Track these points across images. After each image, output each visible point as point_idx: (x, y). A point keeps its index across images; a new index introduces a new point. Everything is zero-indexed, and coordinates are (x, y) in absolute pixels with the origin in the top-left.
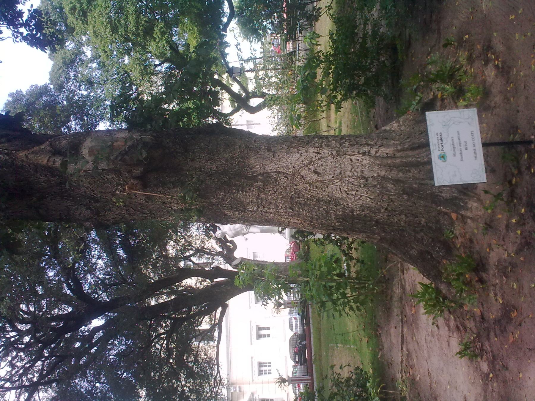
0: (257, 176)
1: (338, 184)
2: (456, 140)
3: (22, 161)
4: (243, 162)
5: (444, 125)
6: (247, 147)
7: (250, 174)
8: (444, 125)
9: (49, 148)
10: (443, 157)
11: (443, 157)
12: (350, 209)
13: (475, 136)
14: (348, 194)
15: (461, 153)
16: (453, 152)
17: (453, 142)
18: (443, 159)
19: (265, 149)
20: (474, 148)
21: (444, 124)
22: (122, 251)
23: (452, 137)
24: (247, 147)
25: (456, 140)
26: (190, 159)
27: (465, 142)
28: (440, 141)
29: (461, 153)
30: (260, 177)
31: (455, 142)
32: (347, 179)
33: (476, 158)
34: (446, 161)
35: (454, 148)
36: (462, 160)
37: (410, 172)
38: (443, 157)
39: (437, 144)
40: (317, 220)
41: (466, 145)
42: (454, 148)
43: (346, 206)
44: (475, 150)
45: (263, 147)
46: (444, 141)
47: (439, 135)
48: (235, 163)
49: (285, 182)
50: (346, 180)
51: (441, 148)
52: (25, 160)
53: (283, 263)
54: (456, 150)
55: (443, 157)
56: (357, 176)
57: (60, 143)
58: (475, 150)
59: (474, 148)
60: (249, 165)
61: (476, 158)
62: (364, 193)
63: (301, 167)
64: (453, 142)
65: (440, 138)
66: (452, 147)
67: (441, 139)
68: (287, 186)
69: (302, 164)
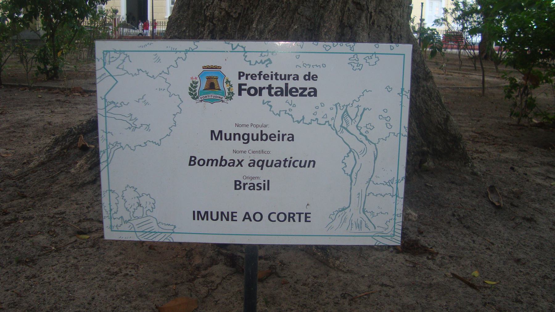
13: (287, 226)
15: (222, 162)
16: (227, 130)
17: (271, 137)
18: (203, 84)
20: (240, 216)
21: (352, 112)
28: (281, 84)
29: (222, 162)
33: (198, 215)
34: (195, 97)
35: (246, 138)
36: (193, 161)
38: (212, 86)
41: (252, 187)
42: (246, 138)
44: (231, 217)
46: (280, 102)
47: (309, 84)
51: (250, 83)
54: (238, 144)
55: (212, 86)
58: (231, 217)
59: (240, 216)
64: (271, 137)
65: (292, 84)
67: (286, 92)
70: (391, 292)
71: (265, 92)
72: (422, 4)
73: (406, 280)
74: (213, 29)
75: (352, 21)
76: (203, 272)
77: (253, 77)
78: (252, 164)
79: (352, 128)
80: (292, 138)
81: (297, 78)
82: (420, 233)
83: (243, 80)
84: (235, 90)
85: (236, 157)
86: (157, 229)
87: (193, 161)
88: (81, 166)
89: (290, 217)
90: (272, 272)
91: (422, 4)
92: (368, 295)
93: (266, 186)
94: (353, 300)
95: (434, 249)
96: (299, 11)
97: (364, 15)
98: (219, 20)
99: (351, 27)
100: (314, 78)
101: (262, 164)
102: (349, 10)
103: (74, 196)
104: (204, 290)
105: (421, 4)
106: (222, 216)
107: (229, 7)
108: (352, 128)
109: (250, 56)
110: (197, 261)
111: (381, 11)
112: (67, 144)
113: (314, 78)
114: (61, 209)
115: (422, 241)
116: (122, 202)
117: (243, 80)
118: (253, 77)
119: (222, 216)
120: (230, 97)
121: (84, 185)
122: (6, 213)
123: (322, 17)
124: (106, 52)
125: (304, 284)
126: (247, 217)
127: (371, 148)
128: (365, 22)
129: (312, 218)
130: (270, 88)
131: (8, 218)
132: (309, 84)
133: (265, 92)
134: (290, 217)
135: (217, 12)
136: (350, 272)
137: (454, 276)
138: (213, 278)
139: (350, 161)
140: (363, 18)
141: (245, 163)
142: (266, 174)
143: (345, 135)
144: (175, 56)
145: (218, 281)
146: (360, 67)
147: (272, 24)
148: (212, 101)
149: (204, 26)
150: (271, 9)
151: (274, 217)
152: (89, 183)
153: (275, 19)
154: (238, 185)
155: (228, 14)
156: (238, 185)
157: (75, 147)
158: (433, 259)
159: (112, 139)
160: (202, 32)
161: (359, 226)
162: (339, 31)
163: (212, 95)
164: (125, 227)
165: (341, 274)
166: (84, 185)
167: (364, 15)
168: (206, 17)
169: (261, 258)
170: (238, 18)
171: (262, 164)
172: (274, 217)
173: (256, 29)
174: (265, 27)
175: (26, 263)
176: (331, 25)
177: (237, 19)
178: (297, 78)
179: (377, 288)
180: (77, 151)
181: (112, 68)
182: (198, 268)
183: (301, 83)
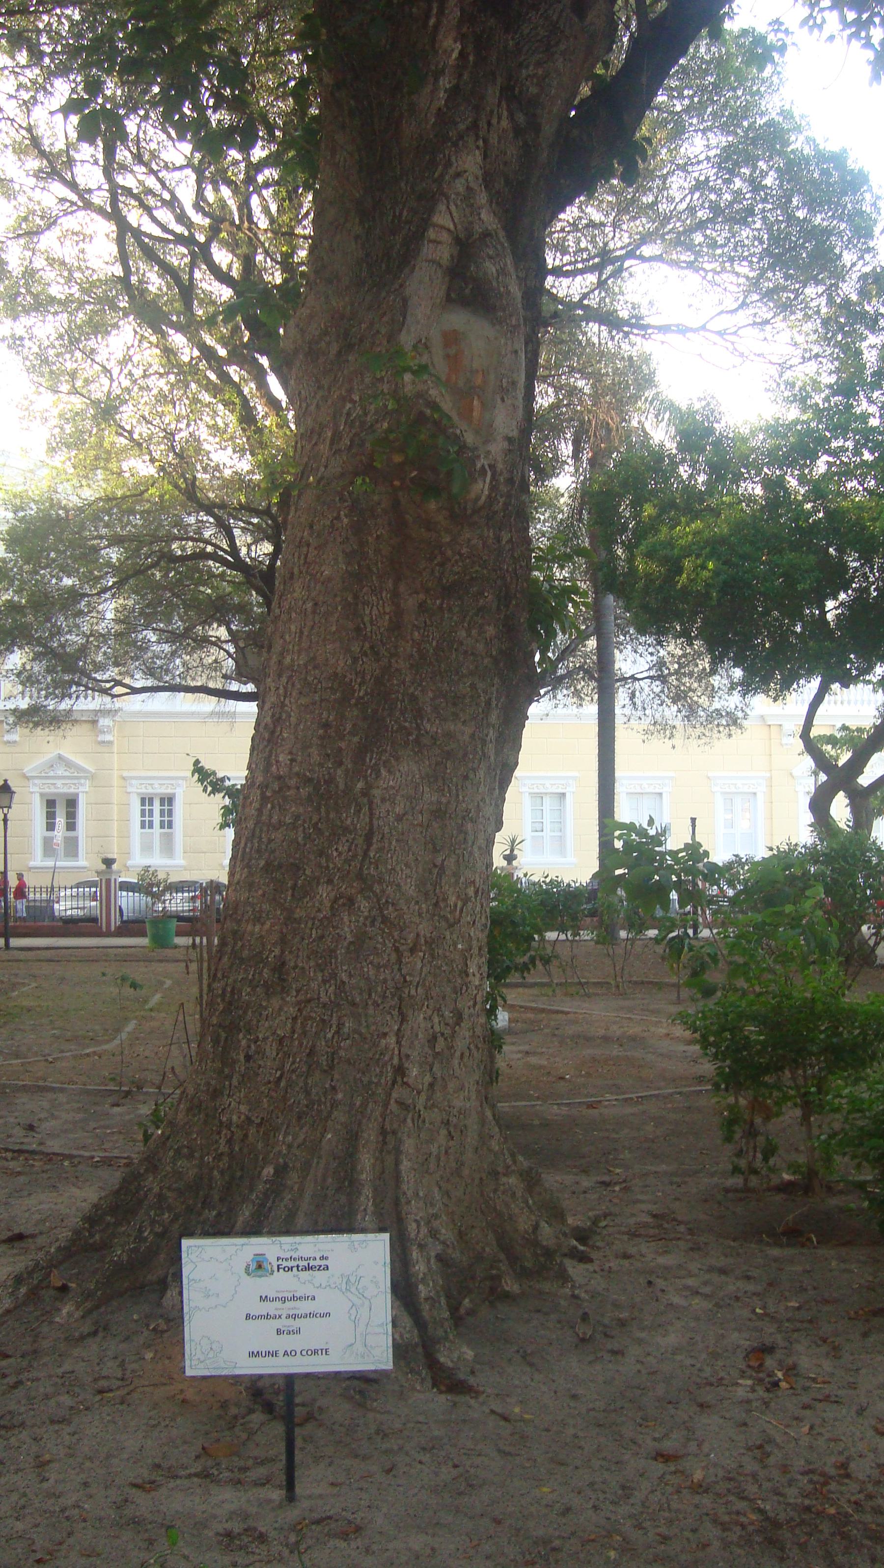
0: (365, 777)
1: (322, 994)
2: (304, 1307)
3: (448, 164)
4: (407, 743)
5: (348, 1280)
6: (449, 755)
7: (370, 759)
8: (348, 1280)
9: (478, 229)
10: (259, 1266)
11: (259, 1266)
12: (255, 1022)
13: (314, 1359)
14: (295, 1019)
15: (268, 1317)
16: (272, 1295)
17: (300, 1298)
18: (253, 1266)
19: (440, 803)
20: (281, 1353)
21: (353, 1279)
22: (864, 357)
23: (314, 1298)
24: (449, 755)
25: (304, 1307)
26: (425, 602)
27: (299, 1331)
28: (305, 1263)
29: (268, 1317)
30: (360, 785)
31: (298, 1304)
32: (334, 1021)
33: (252, 1354)
34: (249, 1274)
35: (284, 1300)
36: (248, 1317)
37: (339, 1190)
38: (260, 1266)
39: (295, 1255)
40: (235, 933)
41: (289, 1333)
42: (284, 1300)
43: (265, 1013)
44: (275, 1354)
45: (444, 800)
46: (305, 1275)
47: (323, 1263)
48: (406, 721)
49: (340, 854)
50: (332, 1016)
51: (285, 1264)
52: (451, 171)
53: (813, 855)
54: (278, 1304)
55: (260, 1266)
56: (340, 1048)
57: (490, 257)
58: (275, 1354)
59: (281, 1353)
60: (397, 759)
61: (252, 1354)
62: (294, 1063)
63: (378, 900)
64: (300, 1298)
65: (312, 1263)
66: (286, 1295)
67: (309, 1268)
68: (329, 858)
69: (387, 902)
70: (425, 1427)
71: (295, 1269)
72: (693, 820)
73: (441, 1417)
74: (231, 1138)
75: (395, 1126)
76: (242, 1421)
77: (286, 1259)
78: (288, 1317)
79: (353, 1290)
80: (314, 1298)
81: (315, 1259)
82: (473, 1372)
83: (280, 1262)
84: (276, 1269)
85: (277, 1313)
86: (223, 1365)
87: (248, 1317)
88: (70, 1314)
89: (315, 1352)
90: (309, 1417)
91: (693, 820)
92: (401, 1431)
93: (299, 1331)
94: (386, 1435)
95: (481, 1389)
96: (333, 1117)
97: (410, 1115)
98: (237, 1126)
99: (394, 1133)
100: (327, 1258)
101: (295, 1317)
102: (391, 1112)
103: (76, 1352)
104: (244, 1436)
105: (689, 822)
106: (269, 1354)
107: (250, 1110)
108: (353, 1290)
109: (284, 1247)
110: (234, 1411)
111: (433, 1105)
112: (35, 1282)
113: (327, 1258)
114: (67, 1367)
115: (472, 1381)
116: (199, 1347)
117: (280, 1262)
118: (286, 1259)
119: (269, 1354)
120: (272, 1273)
121: (82, 1338)
122: (4, 1376)
123: (360, 1124)
124: (189, 1247)
125: (341, 1425)
126: (286, 1353)
127: (367, 1303)
128: (411, 1125)
129: (330, 1352)
130: (298, 1266)
131: (11, 1380)
132: (323, 1263)
133: (295, 1269)
134: (315, 1352)
135: (235, 1118)
136: (388, 1412)
137: (493, 1412)
138: (252, 1425)
139: (353, 1311)
140: (409, 1121)
141: (283, 1317)
142: (298, 1323)
143: (349, 1294)
144: (235, 1248)
145: (257, 1426)
146: (356, 1250)
147: (302, 1137)
148: (260, 1276)
149: (219, 1133)
150: (299, 1118)
151: (304, 1353)
152: (89, 1335)
153: (304, 1130)
154: (279, 1332)
155: (248, 1119)
156: (279, 1332)
157: (48, 1287)
158: (476, 1398)
159: (192, 1304)
160: (217, 1142)
161: (363, 1357)
162: (381, 1139)
163: (260, 1272)
164: (201, 1366)
165: (378, 1416)
166: (82, 1338)
167: (410, 1115)
168: (221, 1122)
169: (298, 1405)
170: (261, 1123)
171: (295, 1317)
172: (304, 1353)
173: (284, 1142)
174: (294, 1139)
175: (59, 1422)
176: (370, 1135)
177: (260, 1125)
178: (315, 1259)
179: (411, 1425)
180: (52, 1292)
181: (193, 1257)
182: (235, 1417)
183: (318, 1262)
